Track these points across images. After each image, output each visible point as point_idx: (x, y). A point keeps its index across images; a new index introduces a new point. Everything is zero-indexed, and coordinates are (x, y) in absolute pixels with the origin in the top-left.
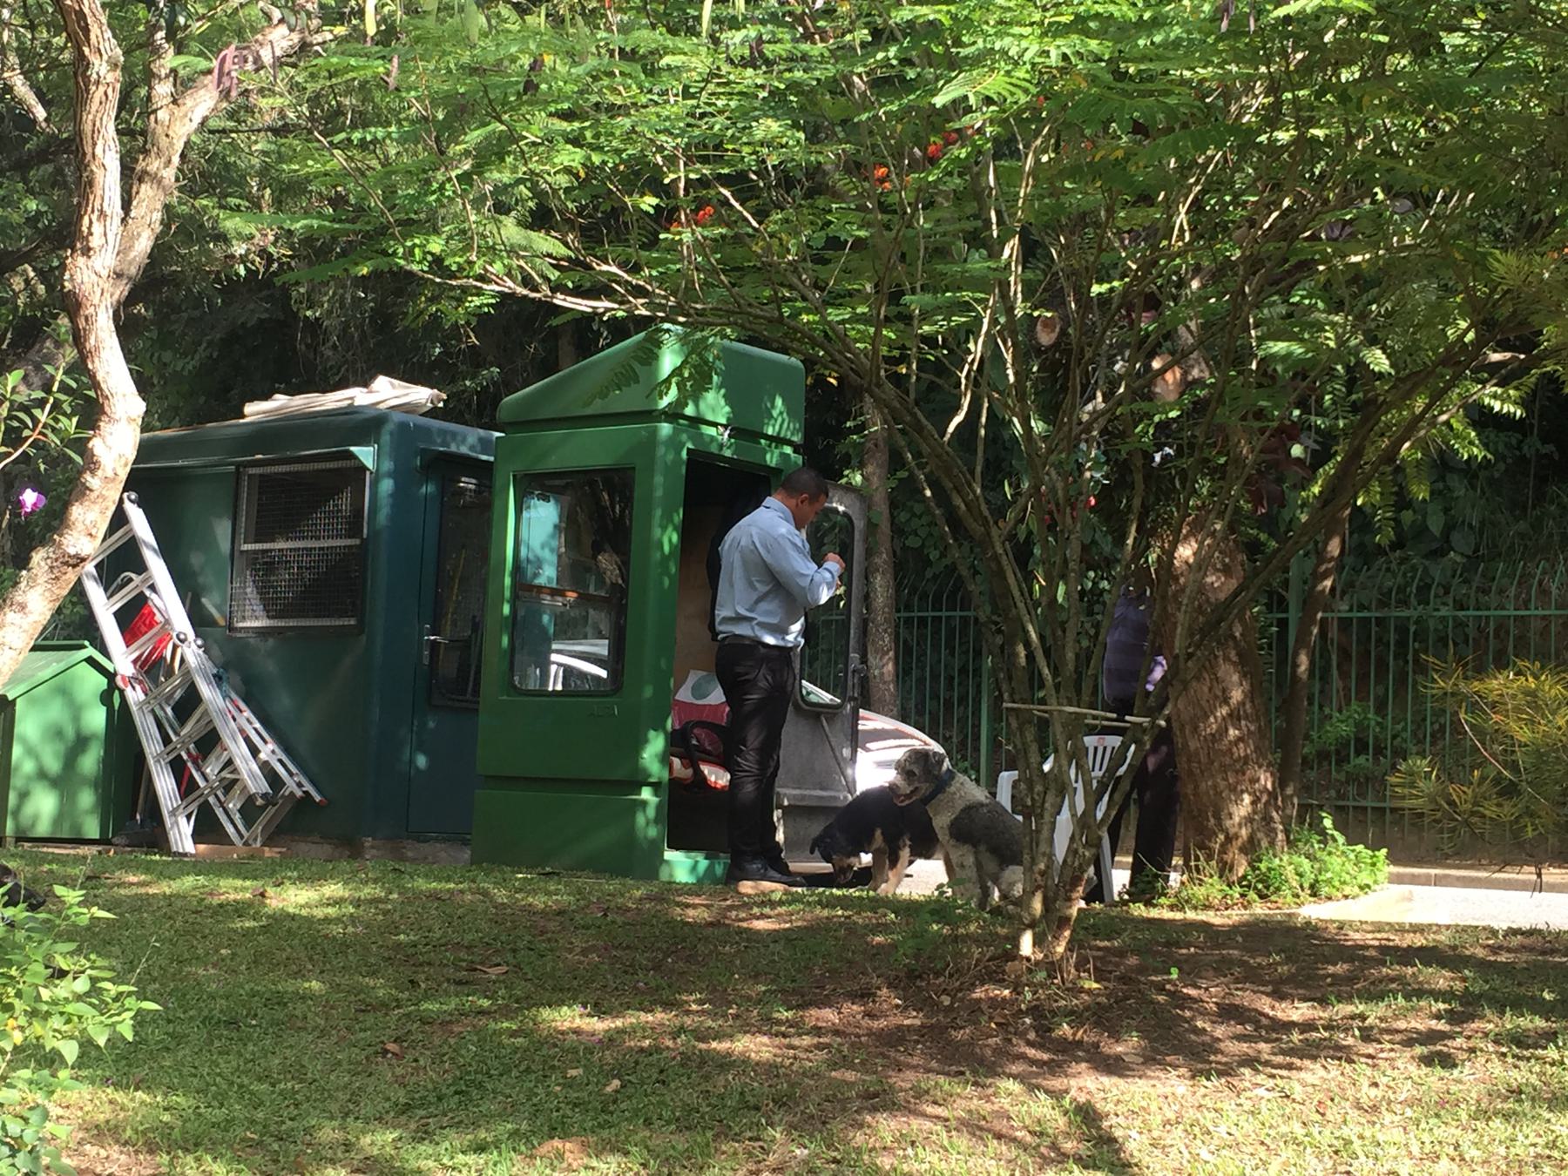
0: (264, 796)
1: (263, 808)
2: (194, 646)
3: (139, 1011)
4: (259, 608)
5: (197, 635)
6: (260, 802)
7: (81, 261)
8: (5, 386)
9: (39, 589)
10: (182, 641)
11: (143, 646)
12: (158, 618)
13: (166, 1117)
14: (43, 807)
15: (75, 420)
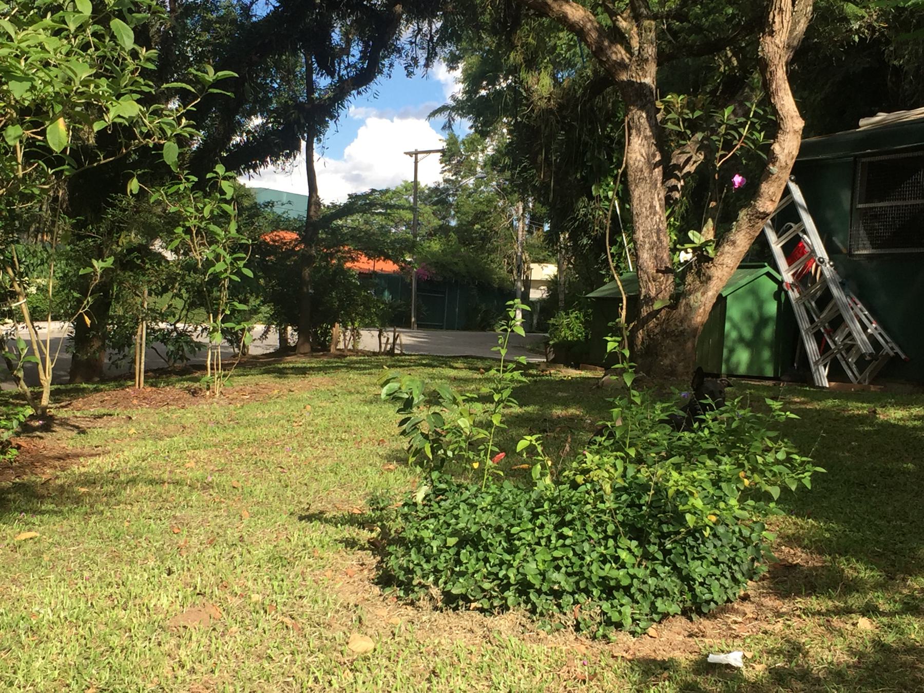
0: (871, 354)
1: (870, 362)
2: (828, 266)
3: (816, 473)
4: (867, 243)
5: (831, 259)
6: (868, 358)
7: (768, 39)
8: (724, 116)
9: (743, 233)
10: (822, 263)
11: (798, 266)
12: (807, 249)
13: (827, 535)
14: (743, 357)
15: (762, 134)
